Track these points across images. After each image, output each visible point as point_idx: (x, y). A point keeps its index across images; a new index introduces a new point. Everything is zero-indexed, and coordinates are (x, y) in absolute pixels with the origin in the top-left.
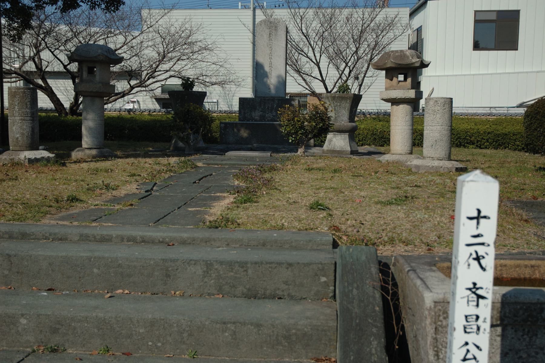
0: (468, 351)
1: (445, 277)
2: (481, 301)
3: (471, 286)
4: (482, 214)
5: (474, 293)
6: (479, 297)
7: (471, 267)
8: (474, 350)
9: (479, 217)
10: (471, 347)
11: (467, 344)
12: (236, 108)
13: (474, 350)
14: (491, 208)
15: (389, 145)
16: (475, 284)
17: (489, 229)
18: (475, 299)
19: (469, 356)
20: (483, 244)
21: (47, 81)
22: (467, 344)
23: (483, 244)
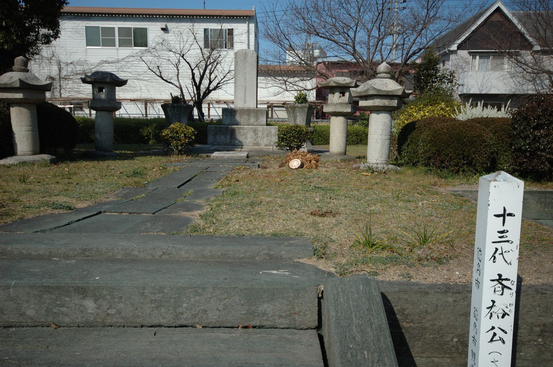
0: (495, 334)
1: (164, 159)
2: (505, 289)
3: (497, 278)
4: (507, 212)
5: (501, 283)
6: (504, 287)
7: (497, 260)
8: (500, 334)
9: (504, 215)
10: (496, 330)
11: (493, 328)
12: (221, 114)
13: (500, 334)
14: (516, 205)
15: (366, 144)
16: (500, 276)
17: (514, 226)
18: (500, 289)
19: (496, 338)
20: (508, 241)
21: (64, 13)
22: (493, 328)
23: (508, 241)
